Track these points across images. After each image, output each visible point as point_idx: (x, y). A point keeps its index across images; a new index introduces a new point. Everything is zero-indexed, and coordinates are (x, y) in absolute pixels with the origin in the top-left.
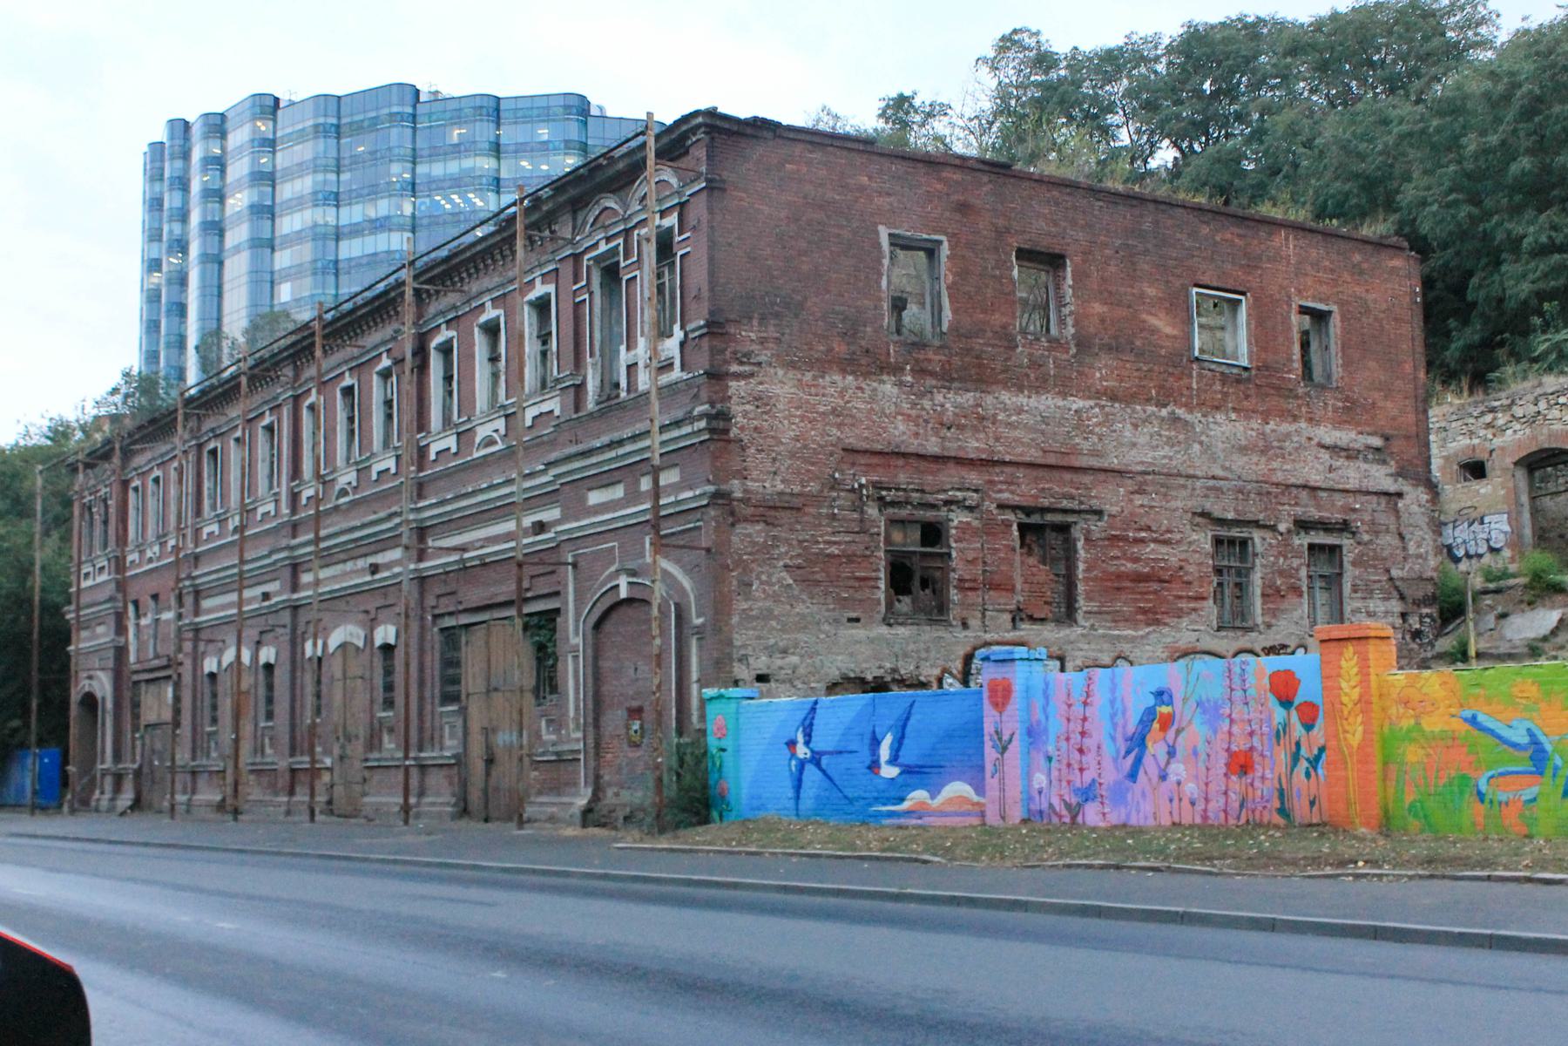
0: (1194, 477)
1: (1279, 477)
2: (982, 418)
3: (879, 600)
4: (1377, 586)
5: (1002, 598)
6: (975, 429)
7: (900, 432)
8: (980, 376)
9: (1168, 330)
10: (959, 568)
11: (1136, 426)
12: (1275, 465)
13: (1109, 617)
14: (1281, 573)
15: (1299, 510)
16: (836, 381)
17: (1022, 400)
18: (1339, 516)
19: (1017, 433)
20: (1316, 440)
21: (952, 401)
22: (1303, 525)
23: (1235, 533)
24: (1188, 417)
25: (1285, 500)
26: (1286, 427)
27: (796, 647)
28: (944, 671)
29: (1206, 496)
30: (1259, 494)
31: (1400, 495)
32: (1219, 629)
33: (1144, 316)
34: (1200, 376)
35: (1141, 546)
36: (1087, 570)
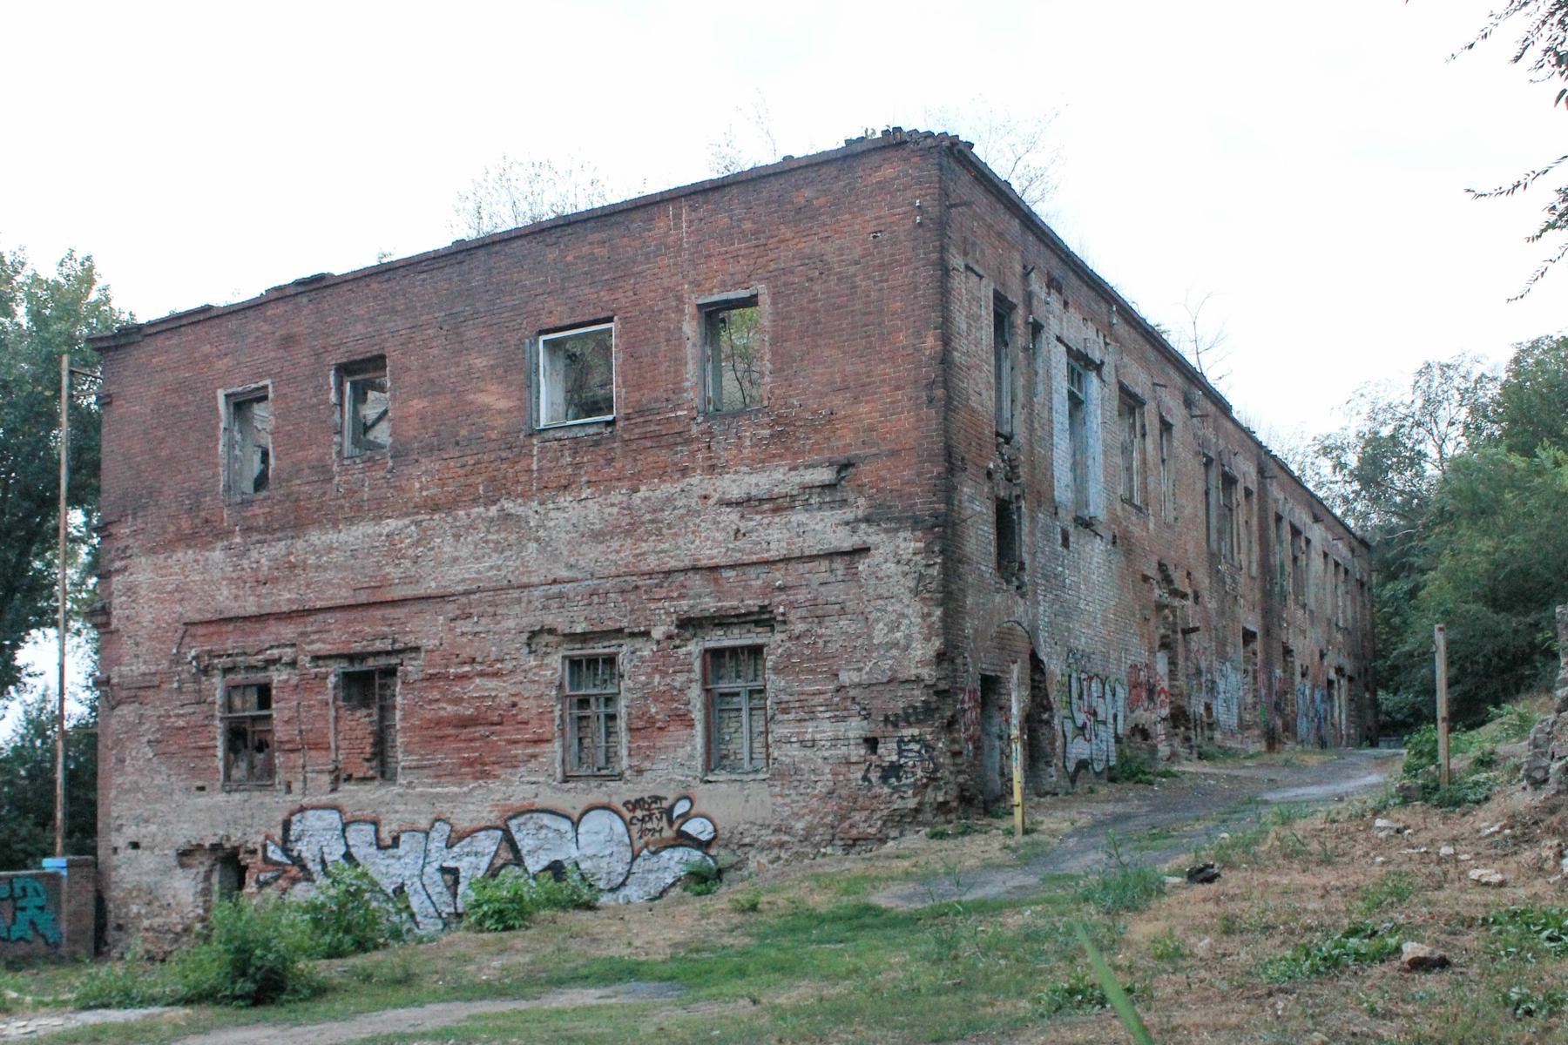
0: (526, 586)
1: (652, 562)
2: (293, 566)
3: (217, 769)
4: (821, 699)
5: (321, 759)
6: (288, 580)
7: (226, 600)
8: (296, 522)
9: (503, 404)
10: (281, 732)
11: (457, 537)
12: (644, 546)
13: (431, 772)
14: (657, 697)
15: (684, 604)
16: (185, 556)
17: (331, 537)
18: (752, 603)
19: (328, 575)
20: (716, 497)
21: (266, 555)
22: (689, 625)
23: (599, 649)
24: (520, 510)
25: (662, 593)
26: (667, 488)
27: (155, 815)
28: (267, 837)
29: (545, 608)
30: (623, 592)
31: (863, 551)
32: (566, 779)
33: (471, 397)
34: (542, 451)
35: (465, 682)
36: (404, 719)
